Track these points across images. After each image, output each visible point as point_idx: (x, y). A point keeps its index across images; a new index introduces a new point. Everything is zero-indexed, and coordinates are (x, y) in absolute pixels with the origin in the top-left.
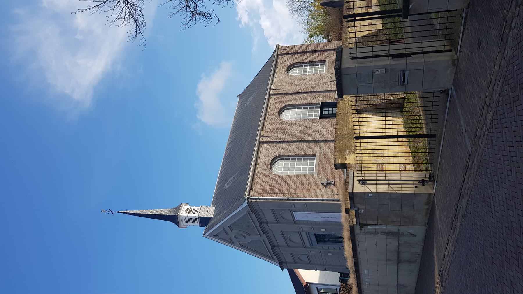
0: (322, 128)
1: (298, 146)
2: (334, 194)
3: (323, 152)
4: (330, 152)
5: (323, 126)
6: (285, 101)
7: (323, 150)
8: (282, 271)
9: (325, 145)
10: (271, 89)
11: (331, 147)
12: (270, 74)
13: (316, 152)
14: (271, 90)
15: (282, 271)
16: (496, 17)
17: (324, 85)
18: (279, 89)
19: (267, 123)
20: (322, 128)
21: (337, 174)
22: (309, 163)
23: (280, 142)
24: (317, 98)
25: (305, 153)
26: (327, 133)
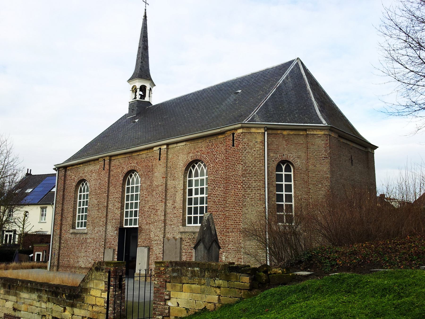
0: (109, 232)
1: (95, 206)
2: (55, 251)
3: (87, 236)
4: (86, 245)
5: (111, 233)
6: (145, 173)
7: (90, 236)
8: (378, 147)
9: (93, 239)
10: (160, 147)
11: (91, 246)
12: (184, 134)
13: (88, 229)
14: (158, 148)
15: (378, 147)
16: (273, 114)
17: (159, 229)
18: (160, 160)
19: (120, 159)
20: (109, 232)
21: (70, 253)
22: (204, 185)
23: (64, 186)
24: (144, 221)
25: (88, 216)
26: (101, 240)
